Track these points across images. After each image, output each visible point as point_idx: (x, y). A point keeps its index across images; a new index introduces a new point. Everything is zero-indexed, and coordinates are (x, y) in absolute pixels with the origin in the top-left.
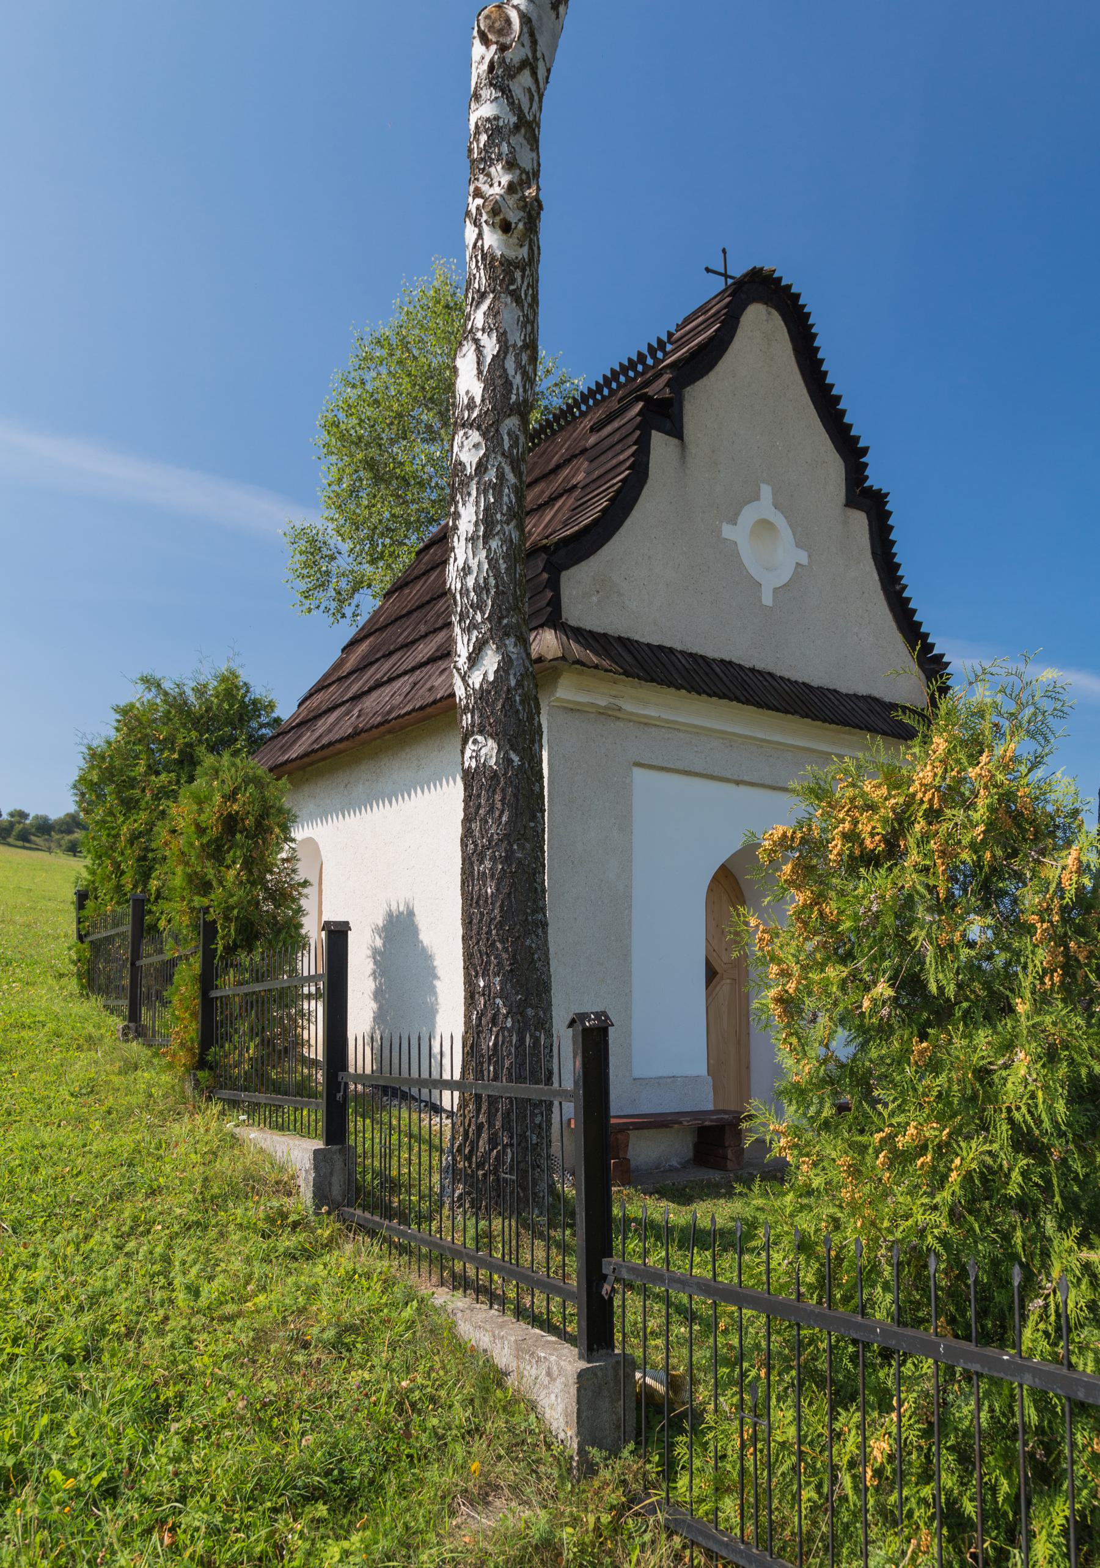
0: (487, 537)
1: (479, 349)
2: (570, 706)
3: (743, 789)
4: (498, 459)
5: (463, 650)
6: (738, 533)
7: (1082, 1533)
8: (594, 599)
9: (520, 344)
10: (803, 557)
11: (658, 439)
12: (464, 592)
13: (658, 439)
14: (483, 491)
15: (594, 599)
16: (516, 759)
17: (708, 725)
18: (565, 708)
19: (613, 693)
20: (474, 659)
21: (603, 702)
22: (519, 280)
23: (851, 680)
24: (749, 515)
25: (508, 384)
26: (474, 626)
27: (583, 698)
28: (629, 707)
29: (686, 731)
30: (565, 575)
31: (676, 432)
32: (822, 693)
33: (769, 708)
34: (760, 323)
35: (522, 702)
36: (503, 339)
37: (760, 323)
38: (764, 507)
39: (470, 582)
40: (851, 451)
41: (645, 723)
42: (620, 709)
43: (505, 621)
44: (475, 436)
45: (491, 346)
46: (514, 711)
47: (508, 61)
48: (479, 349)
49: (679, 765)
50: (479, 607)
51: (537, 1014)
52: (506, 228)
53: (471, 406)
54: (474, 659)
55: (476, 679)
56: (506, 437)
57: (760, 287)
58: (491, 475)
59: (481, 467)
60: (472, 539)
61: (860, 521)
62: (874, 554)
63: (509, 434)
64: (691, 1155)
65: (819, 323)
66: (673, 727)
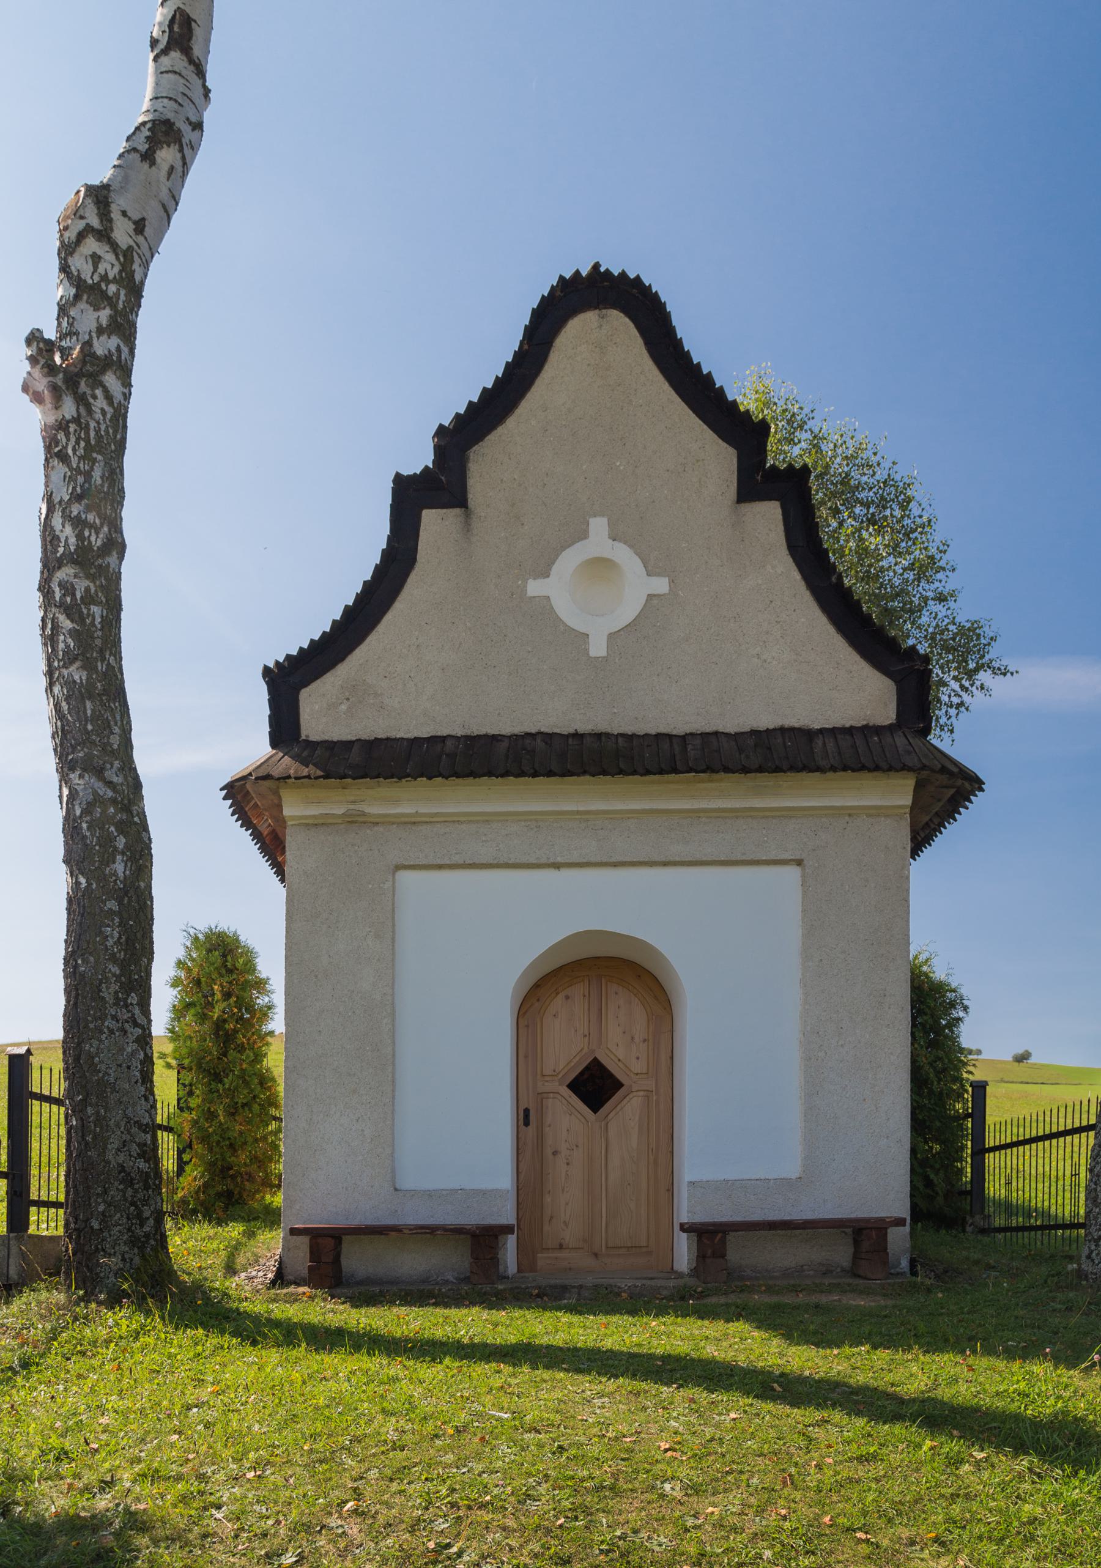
2: (311, 821)
3: (565, 873)
8: (344, 707)
9: (67, 498)
15: (344, 707)
16: (83, 880)
17: (511, 809)
18: (307, 825)
19: (352, 798)
21: (339, 810)
22: (64, 440)
25: (55, 539)
27: (314, 811)
28: (374, 809)
29: (470, 822)
30: (304, 694)
32: (710, 738)
33: (727, 770)
35: (88, 828)
41: (412, 822)
42: (364, 814)
43: (70, 757)
47: (66, 241)
49: (457, 859)
51: (98, 1113)
56: (57, 590)
62: (792, 548)
63: (60, 585)
66: (431, 820)
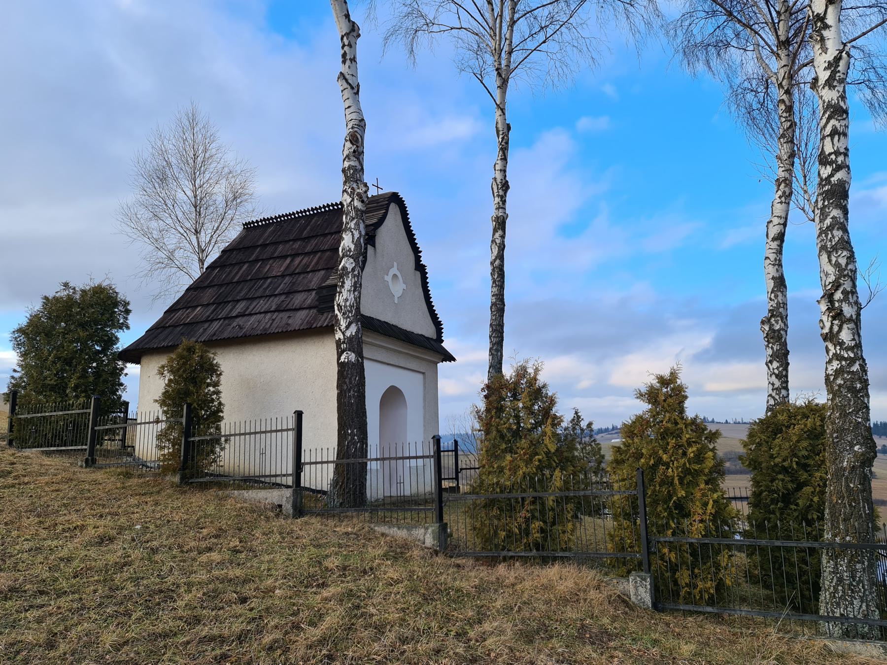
0: (354, 291)
1: (353, 235)
4: (357, 269)
5: (343, 324)
6: (388, 278)
7: (886, 18)
10: (404, 286)
11: (369, 246)
12: (345, 306)
13: (369, 246)
14: (354, 276)
20: (347, 327)
23: (418, 330)
24: (391, 273)
26: (348, 317)
31: (374, 245)
34: (393, 209)
36: (360, 233)
37: (393, 209)
38: (394, 271)
39: (348, 304)
40: (416, 251)
44: (352, 260)
45: (357, 235)
46: (355, 344)
48: (353, 235)
50: (351, 312)
52: (363, 202)
53: (350, 250)
54: (347, 327)
55: (348, 334)
57: (395, 198)
58: (356, 273)
59: (353, 270)
60: (349, 291)
61: (418, 274)
64: (692, 408)
65: (409, 210)
